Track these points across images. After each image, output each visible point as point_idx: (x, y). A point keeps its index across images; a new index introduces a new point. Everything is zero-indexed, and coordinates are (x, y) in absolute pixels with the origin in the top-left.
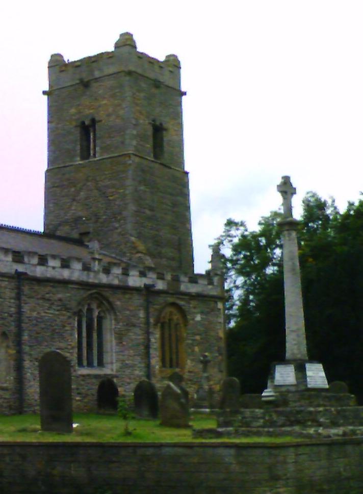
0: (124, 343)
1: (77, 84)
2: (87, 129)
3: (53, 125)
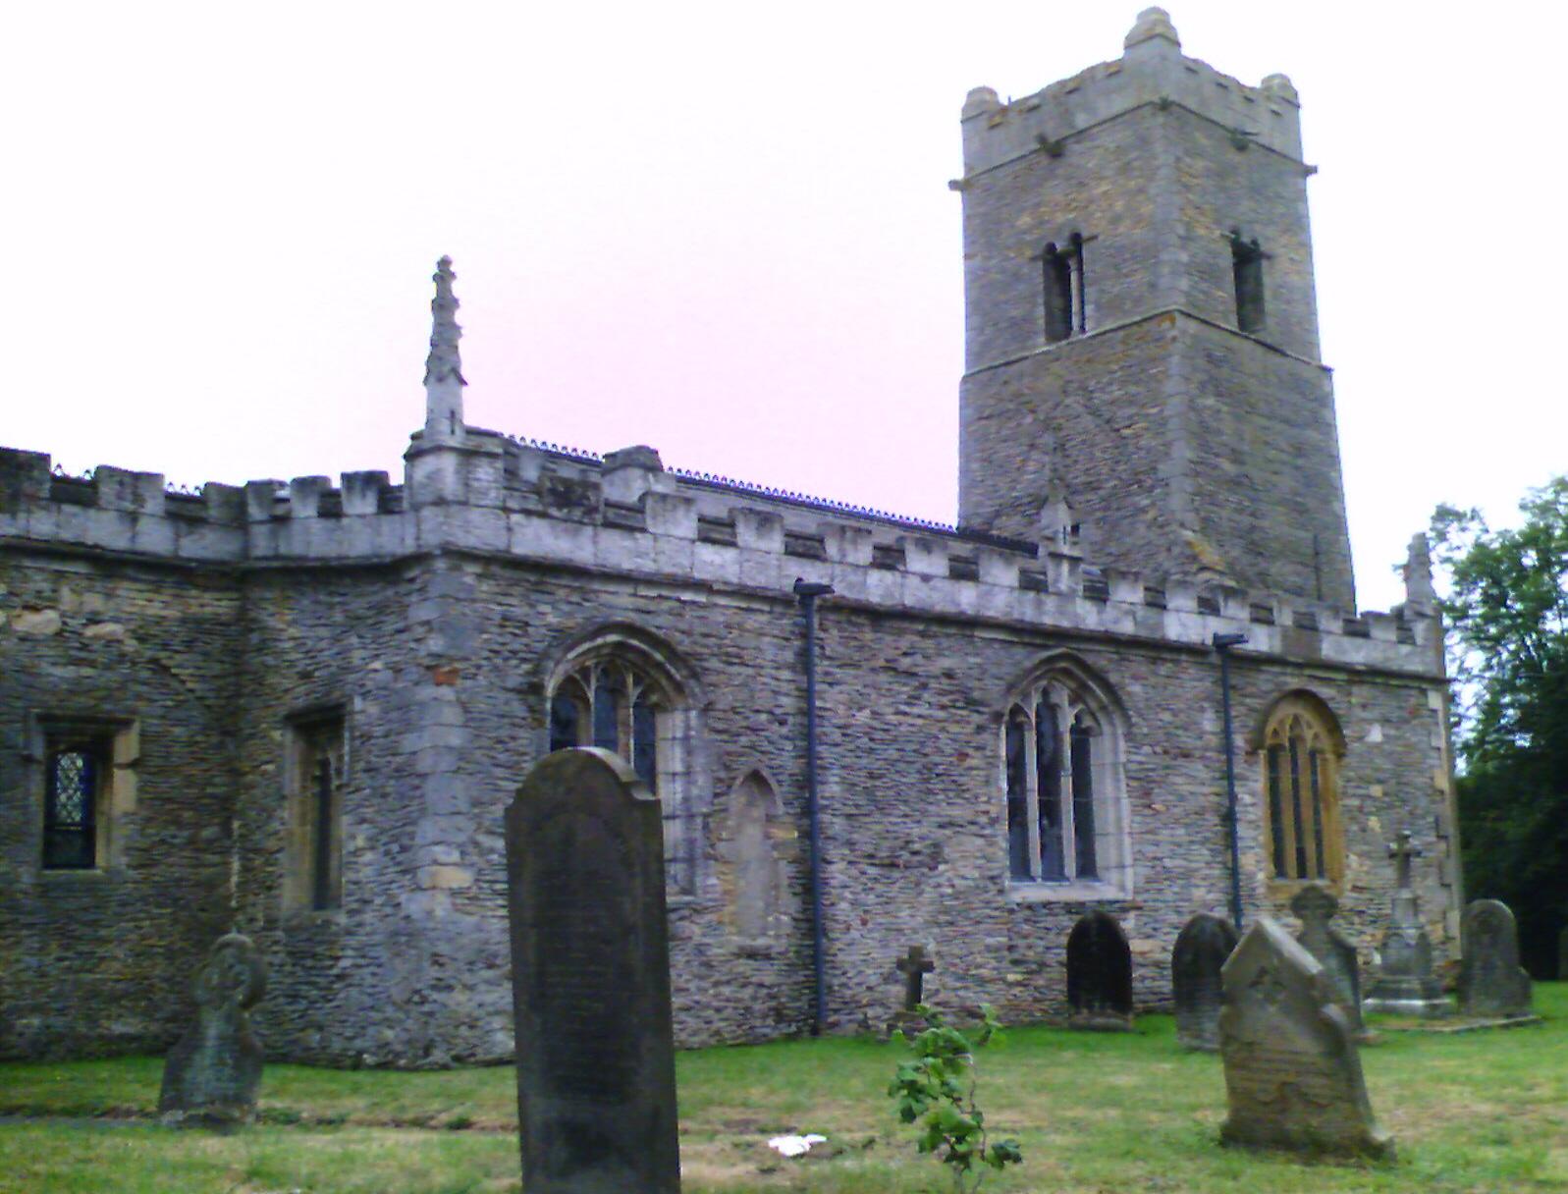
0: (1156, 806)
1: (1035, 151)
2: (1061, 264)
3: (977, 261)
